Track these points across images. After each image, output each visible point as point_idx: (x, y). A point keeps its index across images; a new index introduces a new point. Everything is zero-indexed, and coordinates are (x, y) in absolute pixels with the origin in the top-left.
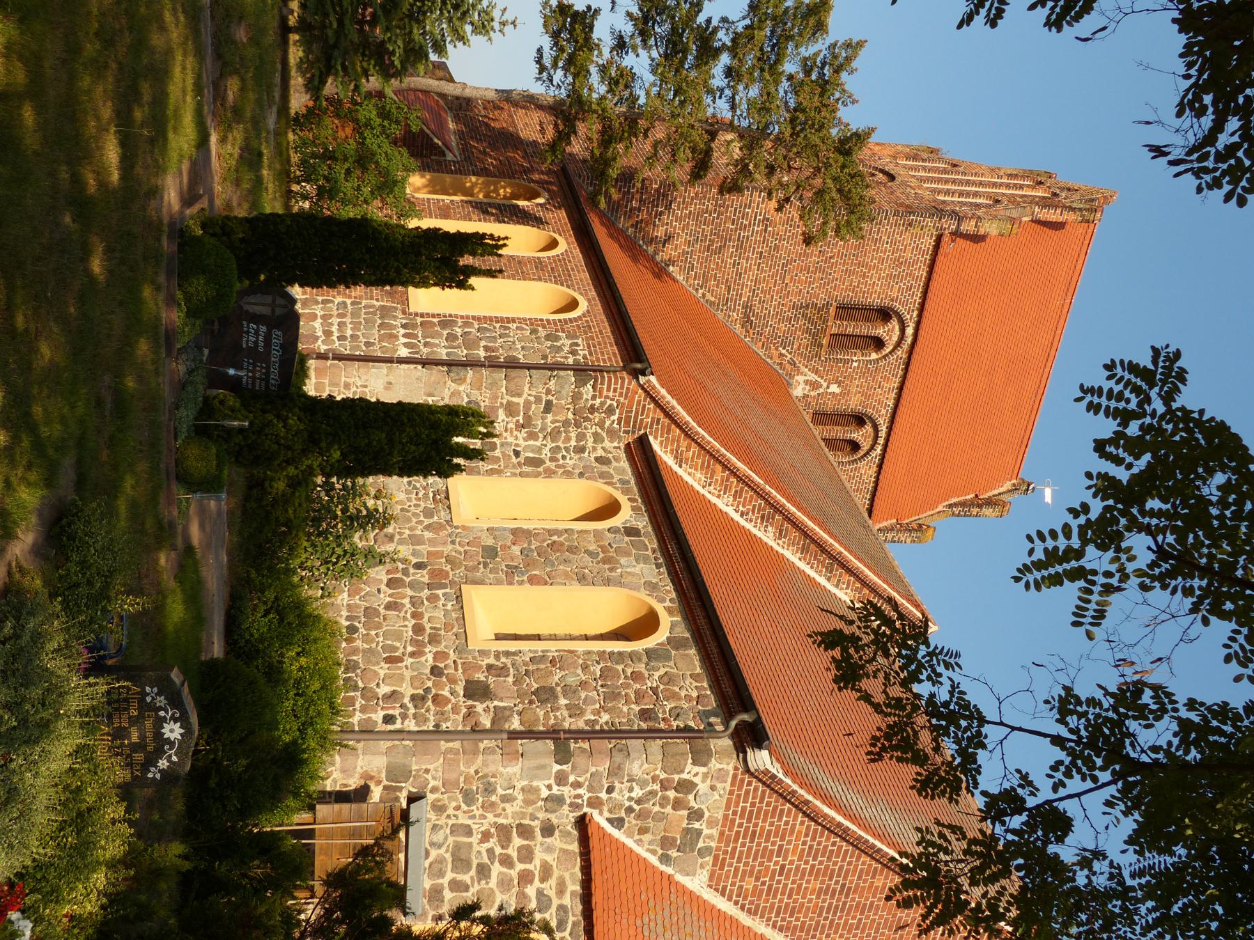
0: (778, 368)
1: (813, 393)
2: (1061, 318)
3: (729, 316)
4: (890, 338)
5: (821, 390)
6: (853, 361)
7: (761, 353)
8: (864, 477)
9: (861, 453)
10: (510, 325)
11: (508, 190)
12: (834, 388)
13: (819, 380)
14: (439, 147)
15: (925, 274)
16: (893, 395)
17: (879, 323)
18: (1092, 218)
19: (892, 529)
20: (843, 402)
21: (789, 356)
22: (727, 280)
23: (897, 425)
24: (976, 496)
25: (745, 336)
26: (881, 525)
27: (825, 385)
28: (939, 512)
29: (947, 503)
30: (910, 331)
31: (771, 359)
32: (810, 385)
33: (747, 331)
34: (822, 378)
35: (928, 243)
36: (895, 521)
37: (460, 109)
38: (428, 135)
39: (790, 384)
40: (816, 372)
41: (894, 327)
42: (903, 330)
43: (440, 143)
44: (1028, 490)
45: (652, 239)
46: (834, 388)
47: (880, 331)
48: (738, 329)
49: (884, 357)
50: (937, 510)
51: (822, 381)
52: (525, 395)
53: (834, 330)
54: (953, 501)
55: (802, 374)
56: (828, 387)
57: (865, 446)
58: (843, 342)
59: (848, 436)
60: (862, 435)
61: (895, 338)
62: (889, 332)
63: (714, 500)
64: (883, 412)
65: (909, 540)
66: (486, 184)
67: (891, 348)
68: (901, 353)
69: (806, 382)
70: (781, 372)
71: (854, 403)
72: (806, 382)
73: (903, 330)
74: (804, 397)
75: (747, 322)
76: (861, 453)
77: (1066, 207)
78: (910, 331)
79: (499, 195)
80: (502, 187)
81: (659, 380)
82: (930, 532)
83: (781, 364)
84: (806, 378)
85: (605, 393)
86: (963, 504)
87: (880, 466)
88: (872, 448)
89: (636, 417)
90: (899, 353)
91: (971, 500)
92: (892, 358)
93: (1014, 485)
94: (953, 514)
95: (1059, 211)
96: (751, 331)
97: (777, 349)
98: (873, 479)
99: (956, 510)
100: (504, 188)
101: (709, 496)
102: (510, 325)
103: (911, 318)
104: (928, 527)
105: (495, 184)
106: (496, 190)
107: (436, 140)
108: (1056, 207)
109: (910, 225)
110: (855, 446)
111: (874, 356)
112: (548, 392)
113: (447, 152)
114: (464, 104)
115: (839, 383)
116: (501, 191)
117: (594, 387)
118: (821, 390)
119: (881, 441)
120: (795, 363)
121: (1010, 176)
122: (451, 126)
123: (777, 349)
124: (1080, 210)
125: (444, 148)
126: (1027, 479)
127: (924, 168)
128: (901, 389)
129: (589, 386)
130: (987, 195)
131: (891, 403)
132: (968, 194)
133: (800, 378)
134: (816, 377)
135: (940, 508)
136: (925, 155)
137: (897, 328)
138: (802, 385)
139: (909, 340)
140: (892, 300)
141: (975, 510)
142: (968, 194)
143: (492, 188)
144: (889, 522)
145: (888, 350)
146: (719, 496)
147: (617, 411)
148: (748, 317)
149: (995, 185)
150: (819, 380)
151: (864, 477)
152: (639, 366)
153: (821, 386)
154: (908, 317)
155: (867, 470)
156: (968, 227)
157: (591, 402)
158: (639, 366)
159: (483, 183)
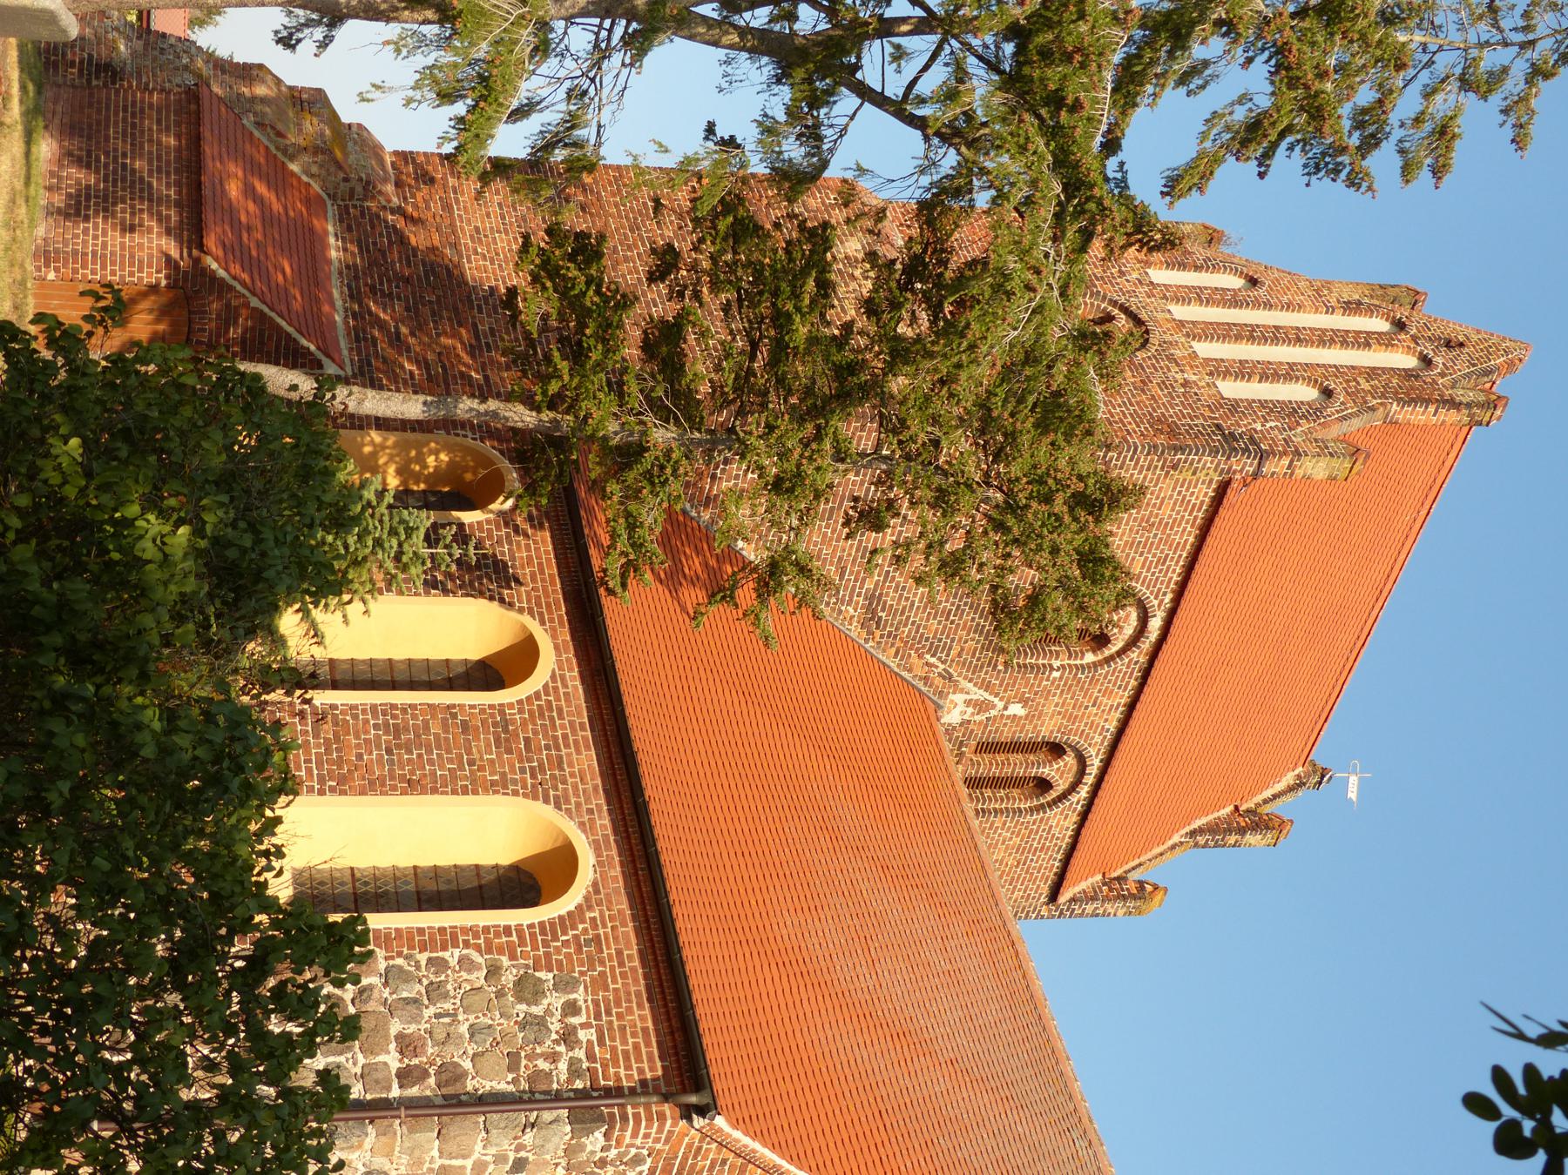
0: (920, 685)
1: (977, 718)
2: (1410, 537)
3: (840, 612)
5: (993, 713)
6: (1052, 668)
7: (893, 664)
8: (1056, 831)
9: (1053, 794)
10: (446, 955)
11: (444, 457)
12: (1016, 709)
13: (991, 698)
14: (311, 354)
15: (1191, 539)
16: (1117, 715)
18: (1487, 419)
19: (1094, 899)
20: (1029, 727)
21: (942, 667)
22: (840, 559)
23: (1117, 763)
24: (1237, 808)
25: (866, 641)
27: (1000, 705)
28: (1173, 847)
29: (1188, 829)
30: (1155, 624)
31: (910, 671)
33: (870, 633)
34: (996, 695)
36: (1099, 877)
37: (351, 197)
38: (288, 335)
39: (938, 707)
40: (988, 687)
41: (1128, 616)
43: (312, 348)
44: (1320, 783)
45: (708, 497)
46: (1016, 709)
48: (855, 631)
49: (1109, 660)
50: (1170, 843)
51: (996, 700)
52: (476, 1156)
54: (1196, 824)
55: (962, 691)
56: (1006, 708)
57: (1061, 785)
59: (1033, 772)
60: (1059, 772)
61: (1129, 631)
64: (1098, 739)
65: (1121, 912)
66: (402, 447)
67: (1119, 645)
68: (1138, 656)
69: (968, 703)
70: (924, 689)
71: (1048, 729)
72: (968, 703)
74: (961, 724)
75: (871, 618)
76: (1053, 794)
77: (1445, 402)
78: (1155, 624)
79: (425, 466)
80: (431, 452)
81: (728, 1120)
82: (1158, 897)
83: (926, 679)
84: (968, 697)
85: (627, 1140)
86: (1212, 829)
87: (1084, 816)
88: (1073, 788)
89: (685, 1158)
91: (1228, 820)
92: (1121, 664)
93: (1299, 776)
94: (1196, 845)
96: (878, 633)
97: (920, 656)
98: (1070, 833)
99: (1201, 840)
100: (437, 453)
102: (446, 955)
104: (1156, 888)
105: (419, 446)
106: (421, 460)
107: (304, 342)
108: (1428, 402)
109: (1174, 467)
110: (1043, 785)
111: (1090, 658)
112: (519, 1148)
113: (325, 361)
114: (359, 189)
115: (1024, 702)
116: (431, 460)
117: (607, 1135)
118: (993, 713)
119: (1089, 780)
120: (951, 676)
122: (335, 252)
124: (1469, 406)
125: (320, 355)
126: (1321, 763)
128: (1131, 707)
129: (599, 1135)
131: (1112, 726)
133: (959, 698)
134: (986, 695)
135: (1176, 839)
137: (1134, 616)
138: (961, 707)
141: (1232, 839)
143: (413, 453)
144: (1090, 881)
147: (649, 1160)
148: (874, 612)
149: (1325, 338)
150: (991, 698)
151: (1056, 831)
152: (693, 1099)
153: (994, 707)
154: (1156, 602)
155: (1062, 821)
157: (599, 1155)
158: (693, 1099)
159: (395, 445)
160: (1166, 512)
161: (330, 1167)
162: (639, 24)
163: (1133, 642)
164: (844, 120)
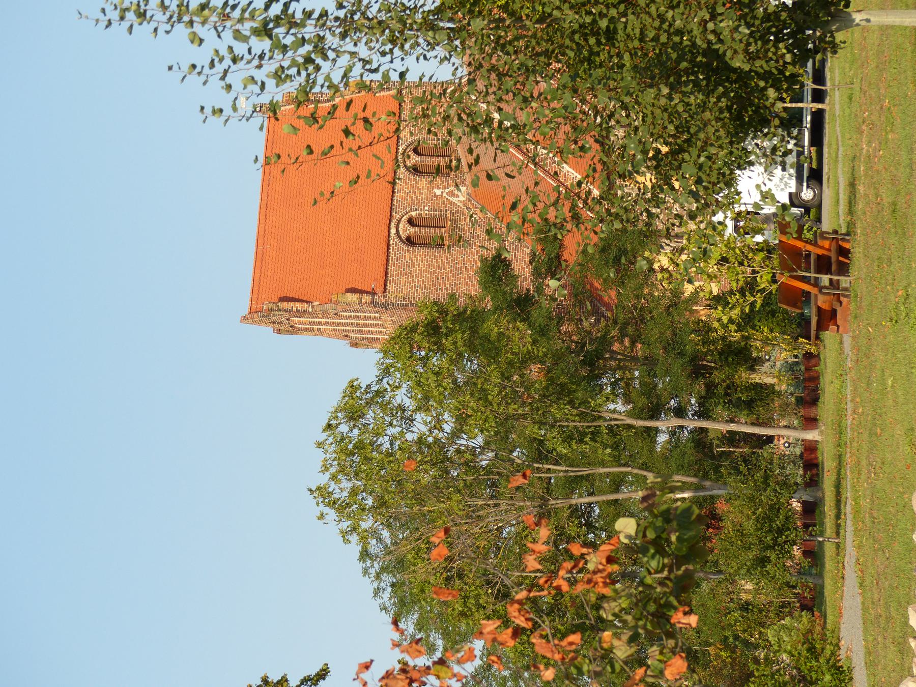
4: (404, 227)
5: (447, 190)
12: (438, 192)
13: (449, 198)
15: (390, 268)
17: (412, 234)
26: (388, 93)
27: (445, 194)
30: (393, 231)
32: (454, 194)
35: (391, 287)
42: (397, 231)
46: (438, 192)
47: (412, 230)
51: (447, 197)
53: (443, 230)
55: (461, 202)
56: (442, 193)
58: (435, 223)
59: (422, 158)
61: (401, 225)
62: (406, 230)
63: (571, 170)
67: (403, 219)
71: (423, 182)
73: (397, 231)
78: (393, 231)
90: (398, 216)
92: (402, 212)
95: (295, 309)
101: (573, 172)
103: (394, 240)
109: (405, 298)
111: (414, 214)
121: (311, 330)
123: (480, 218)
127: (372, 333)
130: (341, 317)
132: (354, 317)
133: (462, 198)
136: (365, 342)
137: (401, 233)
139: (393, 225)
140: (408, 251)
142: (354, 317)
145: (405, 217)
146: (568, 172)
153: (447, 193)
156: (366, 298)
160: (403, 280)
161: (589, 436)
162: (639, 160)
163: (399, 221)
164: (255, 114)
